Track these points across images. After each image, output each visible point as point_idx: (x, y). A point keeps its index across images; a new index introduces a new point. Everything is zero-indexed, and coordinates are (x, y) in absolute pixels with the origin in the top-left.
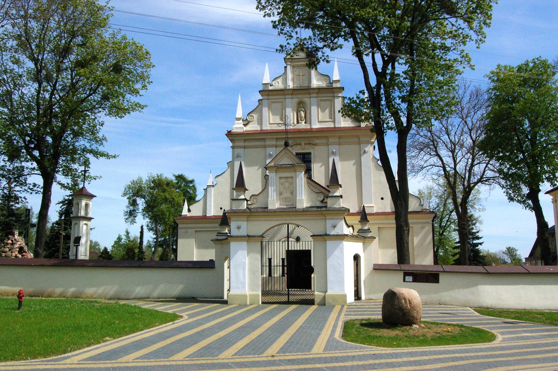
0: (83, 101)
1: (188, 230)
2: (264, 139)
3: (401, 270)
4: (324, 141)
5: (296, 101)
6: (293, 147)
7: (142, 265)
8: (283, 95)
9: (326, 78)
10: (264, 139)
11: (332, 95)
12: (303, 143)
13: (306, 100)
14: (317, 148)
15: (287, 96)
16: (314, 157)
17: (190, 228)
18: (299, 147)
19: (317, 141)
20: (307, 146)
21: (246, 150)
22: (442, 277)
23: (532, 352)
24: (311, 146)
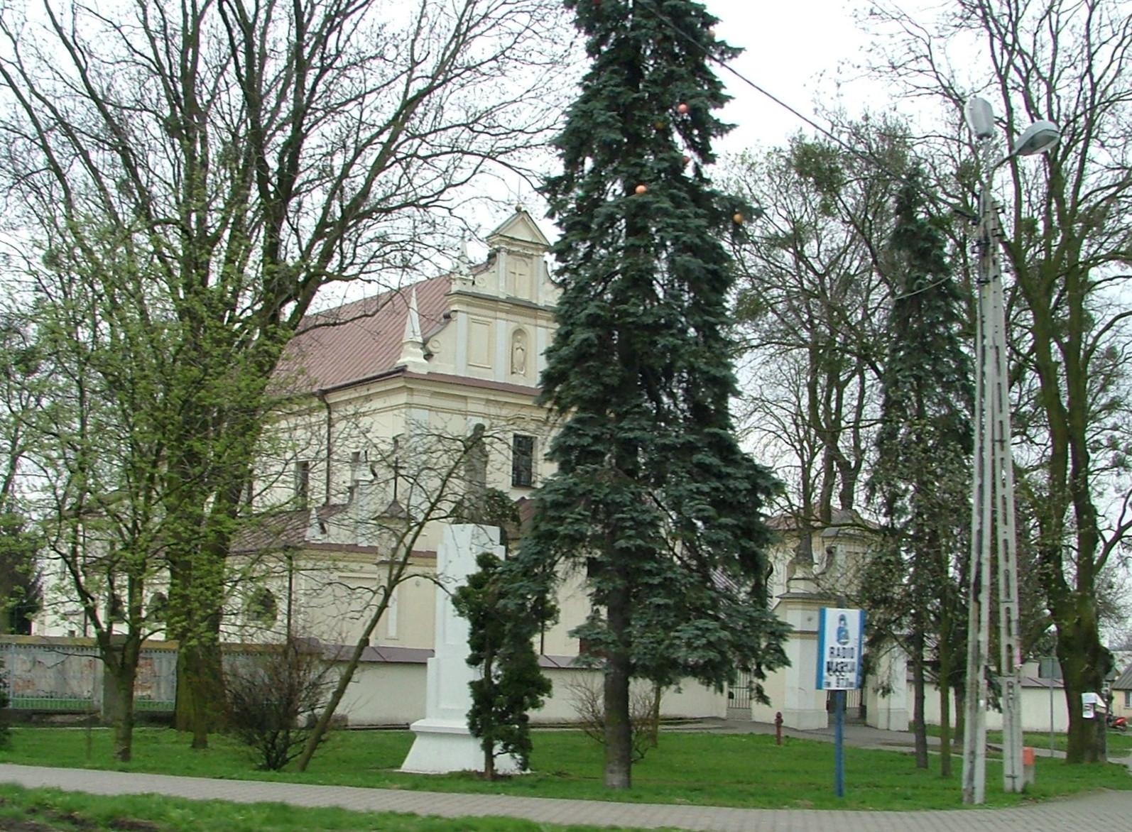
5: (513, 326)
13: (529, 328)
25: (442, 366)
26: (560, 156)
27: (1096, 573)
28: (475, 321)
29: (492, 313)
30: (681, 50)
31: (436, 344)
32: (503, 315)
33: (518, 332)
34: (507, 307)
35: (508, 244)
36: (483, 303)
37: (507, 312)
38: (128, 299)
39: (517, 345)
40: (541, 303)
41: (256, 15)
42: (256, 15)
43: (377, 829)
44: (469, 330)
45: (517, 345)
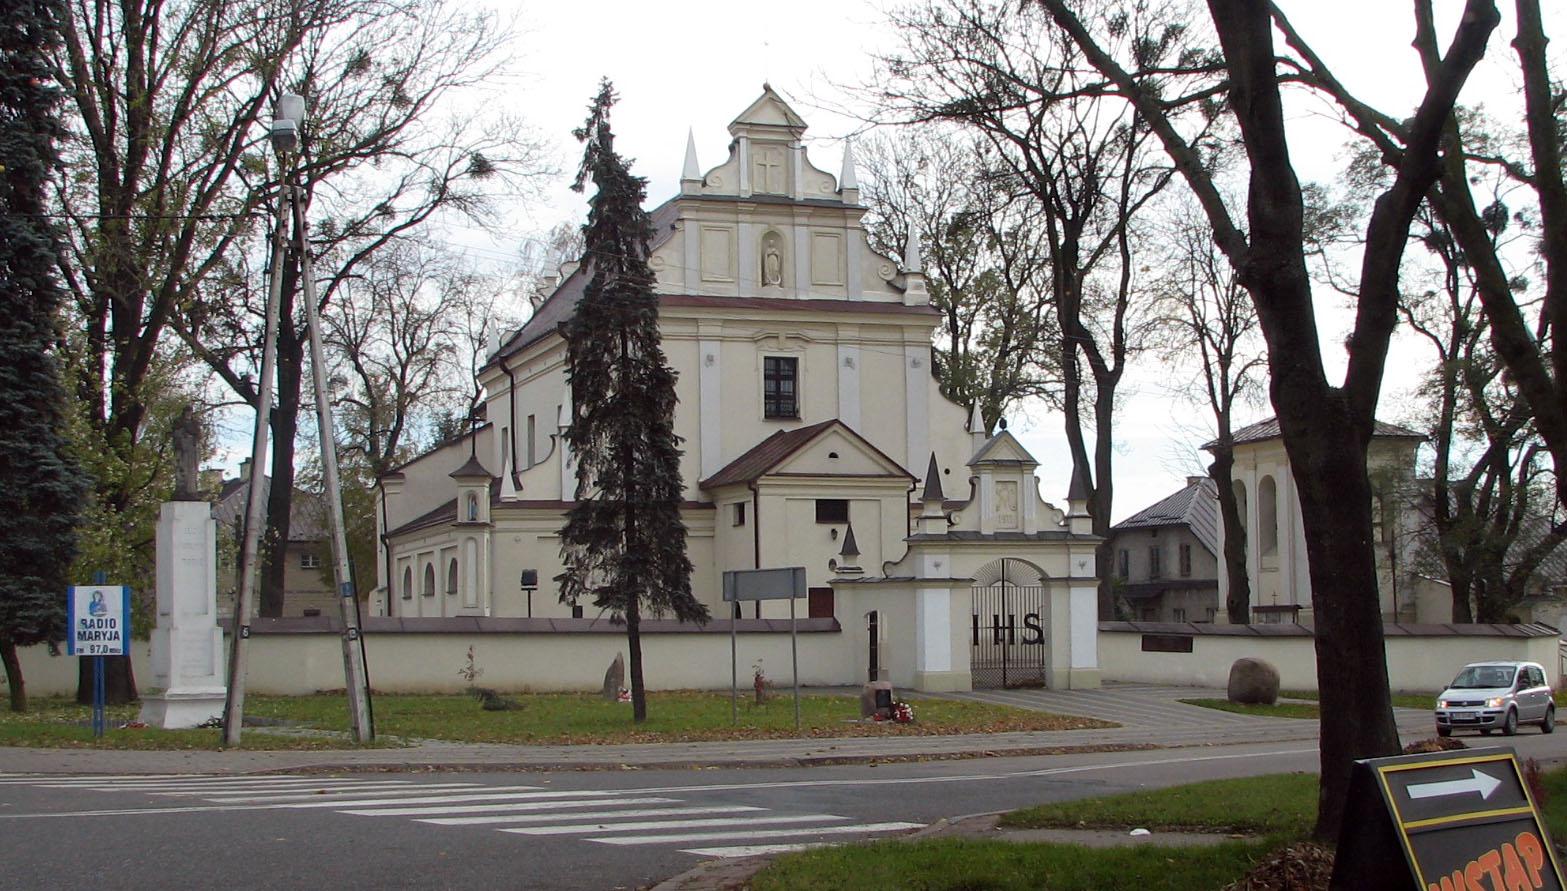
0: (1284, 266)
1: (521, 535)
2: (901, 328)
3: (1139, 632)
4: (828, 334)
5: (760, 229)
6: (760, 343)
7: (707, 628)
8: (731, 213)
9: (826, 179)
10: (901, 328)
11: (840, 222)
12: (782, 338)
13: (785, 230)
14: (811, 349)
15: (741, 217)
16: (806, 370)
17: (529, 531)
18: (773, 343)
19: (812, 334)
20: (790, 344)
21: (725, 344)
22: (1197, 643)
23: (604, 811)
24: (801, 343)
25: (527, 495)
26: (569, 381)
27: (1488, 381)
28: (709, 229)
29: (732, 217)
30: (614, 493)
31: (658, 261)
32: (748, 217)
33: (771, 236)
34: (751, 207)
35: (748, 131)
36: (720, 206)
37: (751, 213)
38: (388, 81)
39: (769, 251)
40: (800, 197)
41: (160, 67)
42: (160, 67)
43: (730, 888)
44: (701, 241)
45: (769, 251)
